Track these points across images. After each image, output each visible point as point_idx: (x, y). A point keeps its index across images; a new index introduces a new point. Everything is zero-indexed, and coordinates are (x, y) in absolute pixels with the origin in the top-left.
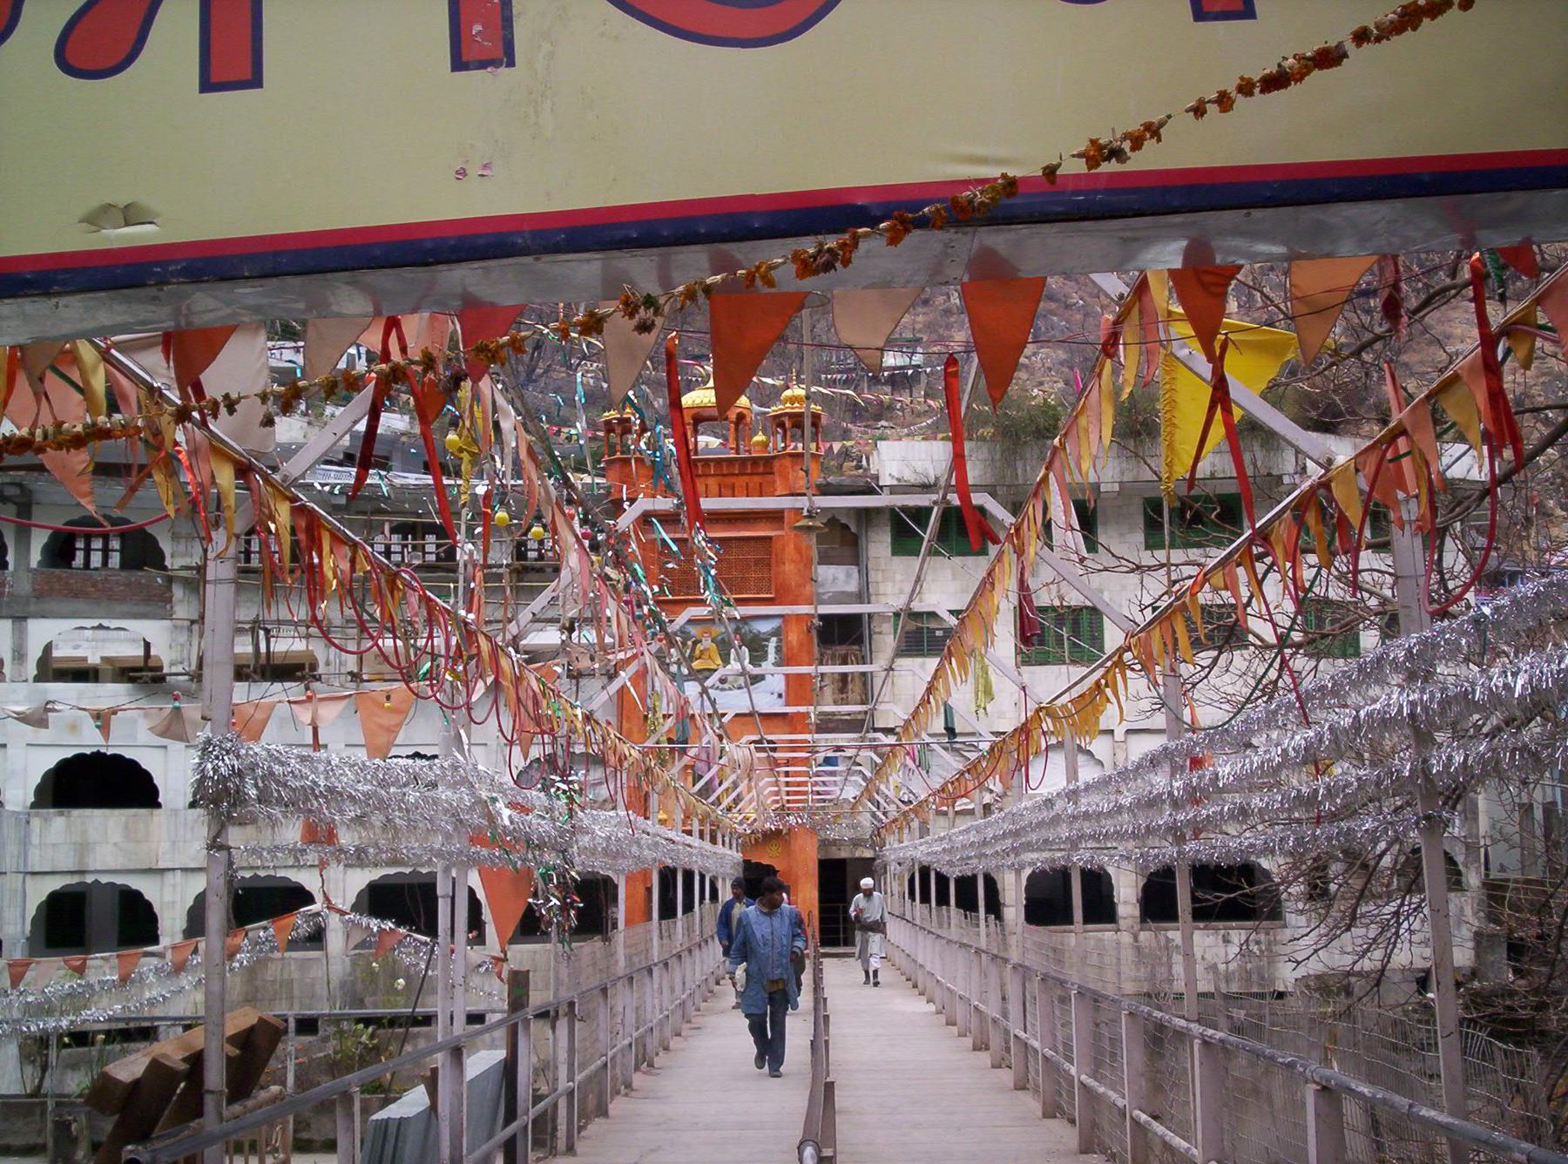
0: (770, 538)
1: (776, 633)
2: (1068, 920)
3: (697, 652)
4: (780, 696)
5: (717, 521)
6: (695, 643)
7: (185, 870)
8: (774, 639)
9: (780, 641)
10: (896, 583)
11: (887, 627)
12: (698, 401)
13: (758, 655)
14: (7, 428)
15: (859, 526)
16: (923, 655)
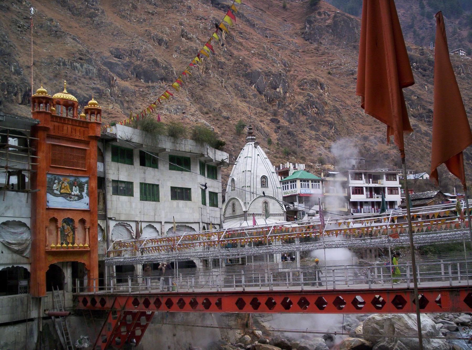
0: (86, 150)
1: (87, 182)
2: (99, 286)
3: (63, 186)
4: (87, 204)
5: (55, 138)
6: (63, 183)
7: (208, 327)
8: (86, 185)
9: (88, 185)
10: (117, 172)
11: (110, 185)
12: (59, 96)
13: (81, 190)
14: (326, 4)
15: (103, 150)
16: (118, 195)
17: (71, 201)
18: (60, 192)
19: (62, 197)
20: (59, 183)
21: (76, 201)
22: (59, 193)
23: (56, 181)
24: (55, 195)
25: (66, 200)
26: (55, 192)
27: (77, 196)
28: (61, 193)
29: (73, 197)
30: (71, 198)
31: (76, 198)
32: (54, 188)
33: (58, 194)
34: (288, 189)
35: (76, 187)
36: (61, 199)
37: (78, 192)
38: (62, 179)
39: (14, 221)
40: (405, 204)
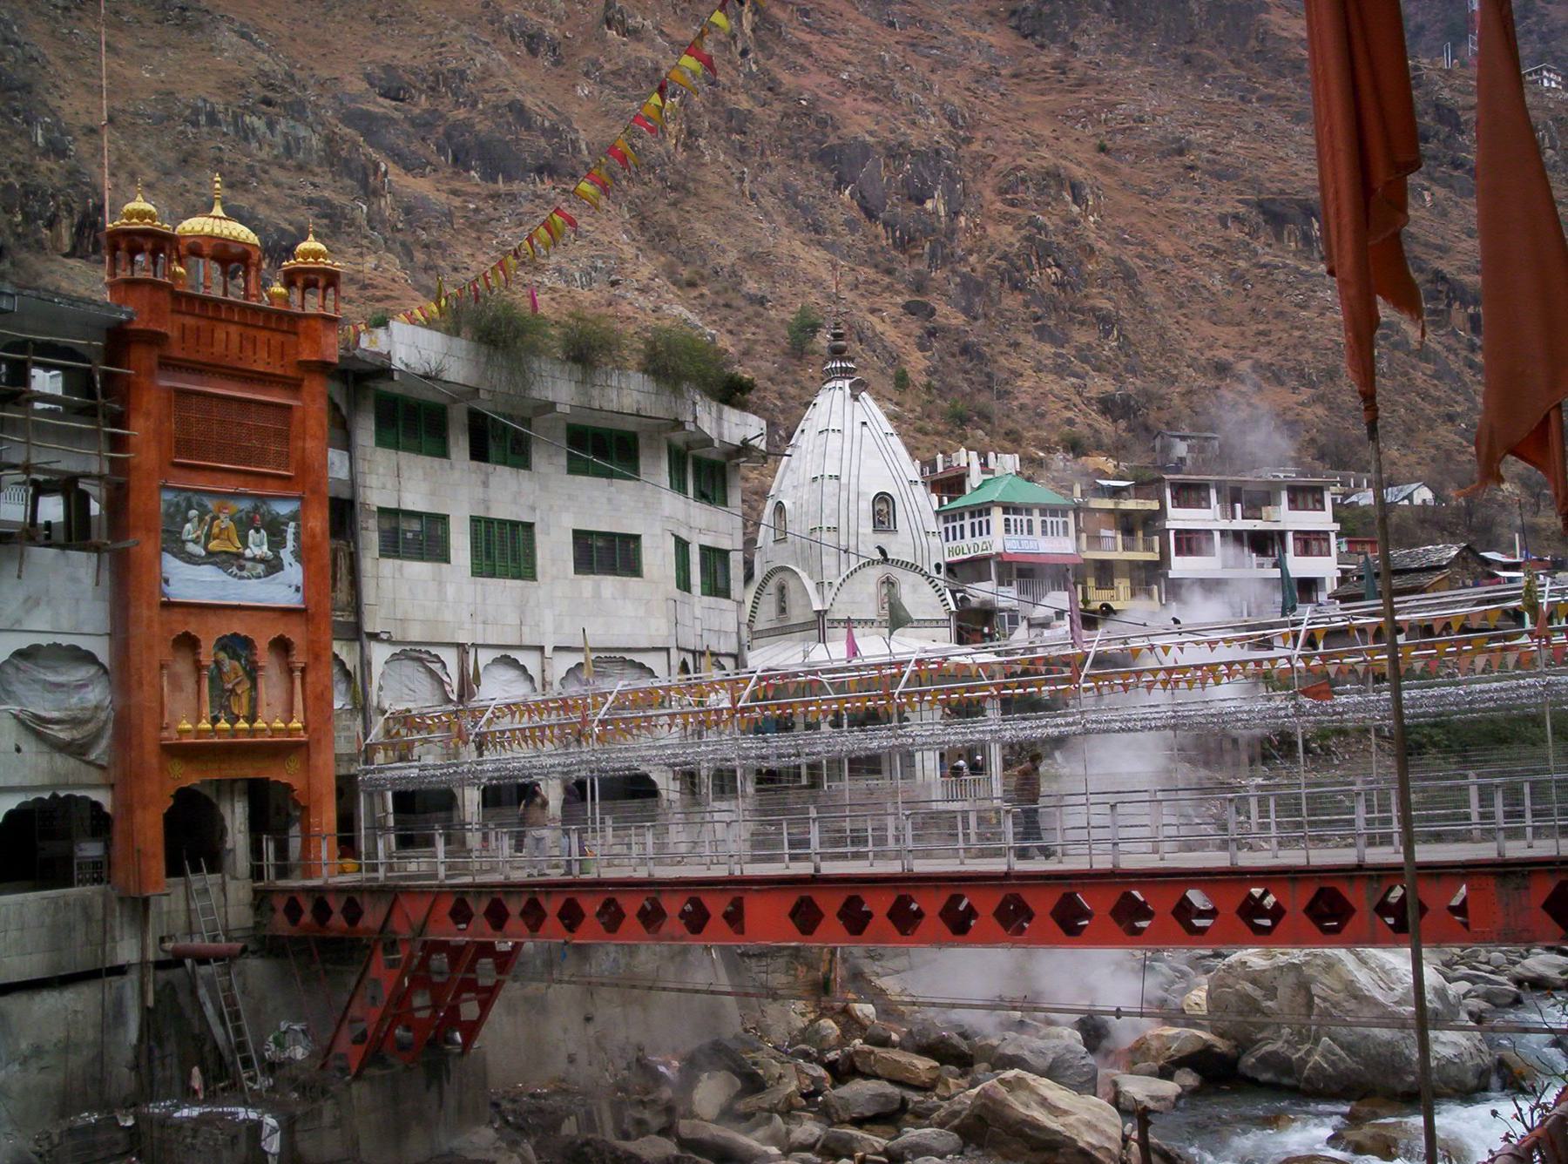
8: (292, 524)
17: (241, 578)
18: (205, 548)
20: (201, 520)
24: (191, 559)
25: (225, 577)
26: (191, 547)
27: (262, 560)
28: (210, 554)
29: (249, 565)
30: (241, 568)
31: (260, 568)
34: (962, 537)
36: (208, 573)
37: (265, 548)
38: (211, 504)
39: (55, 644)
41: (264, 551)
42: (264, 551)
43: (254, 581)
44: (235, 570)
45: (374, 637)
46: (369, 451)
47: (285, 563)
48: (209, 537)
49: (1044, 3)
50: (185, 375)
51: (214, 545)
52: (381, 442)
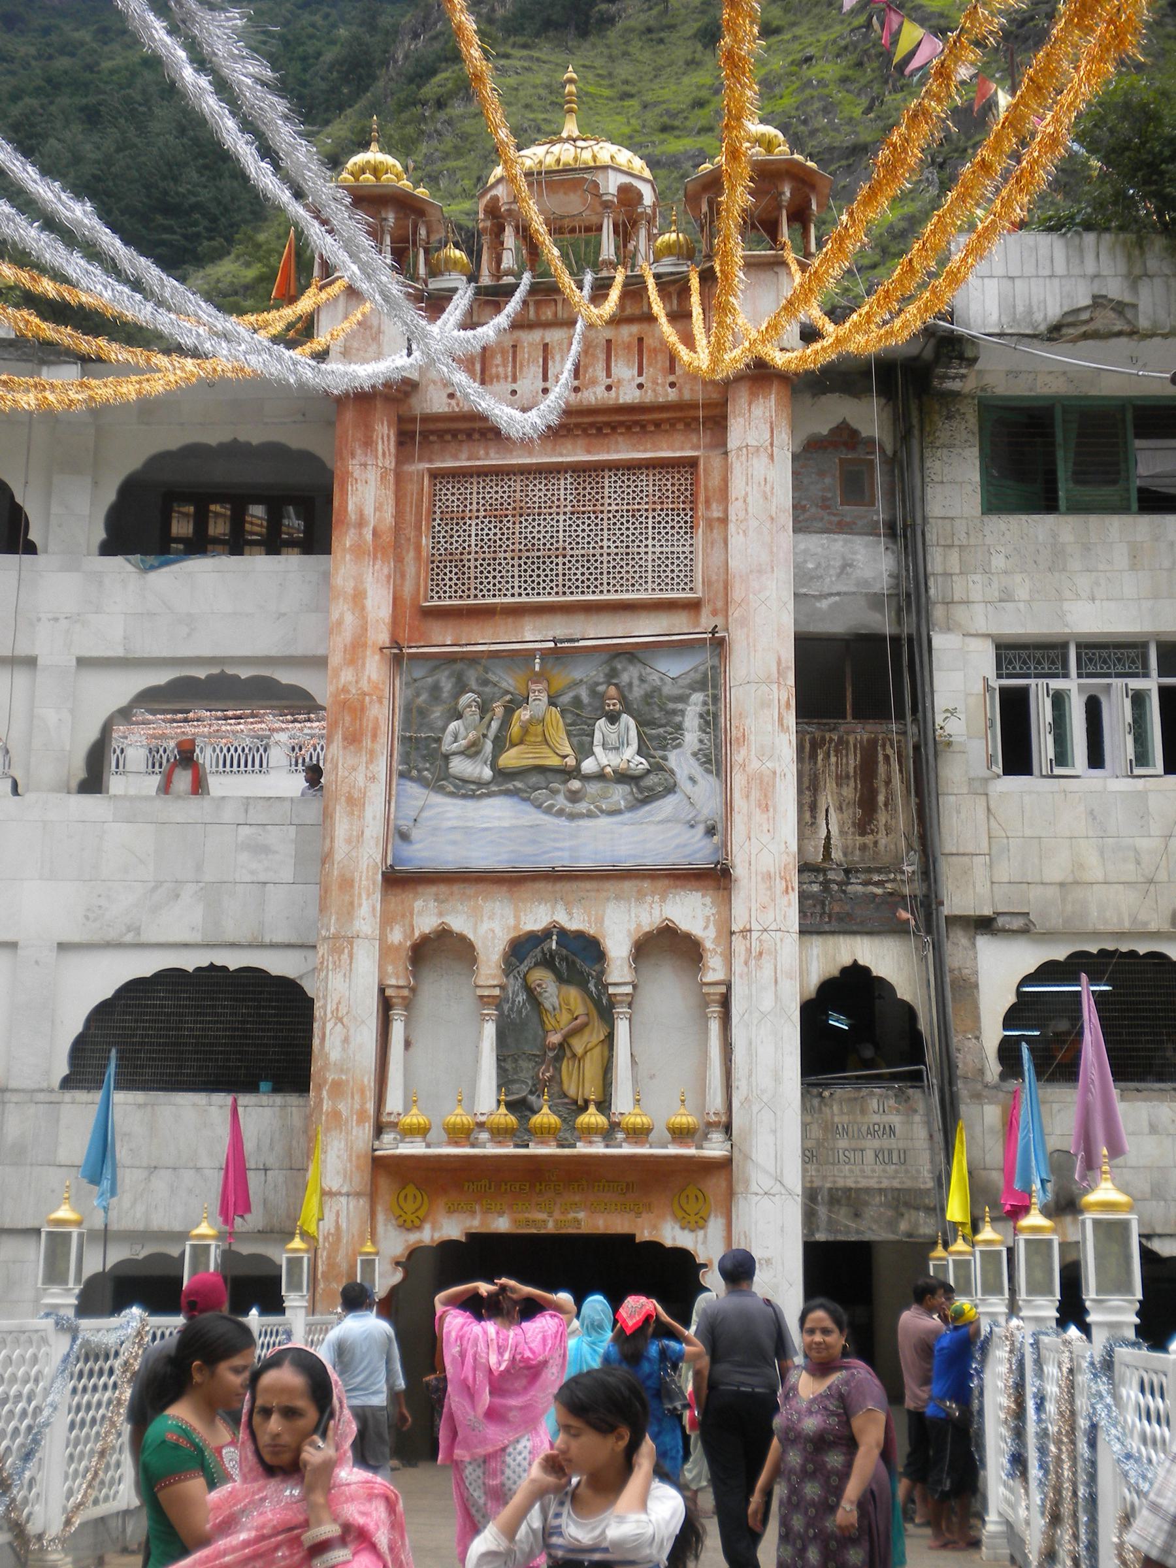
8: (697, 697)
17: (572, 817)
18: (493, 766)
19: (507, 793)
20: (484, 709)
21: (616, 812)
22: (487, 773)
23: (468, 697)
24: (469, 789)
25: (534, 816)
26: (460, 766)
27: (623, 777)
28: (503, 775)
29: (593, 788)
30: (574, 797)
31: (619, 794)
32: (447, 746)
33: (480, 784)
34: (1096, 759)
35: (613, 718)
36: (498, 812)
37: (630, 752)
38: (509, 681)
39: (212, 967)
40: (494, 157)
41: (630, 757)
42: (630, 757)
43: (604, 821)
44: (561, 801)
45: (984, 925)
46: (961, 527)
47: (681, 776)
48: (500, 744)
49: (304, 6)
50: (678, 438)
51: (511, 758)
52: (997, 501)
